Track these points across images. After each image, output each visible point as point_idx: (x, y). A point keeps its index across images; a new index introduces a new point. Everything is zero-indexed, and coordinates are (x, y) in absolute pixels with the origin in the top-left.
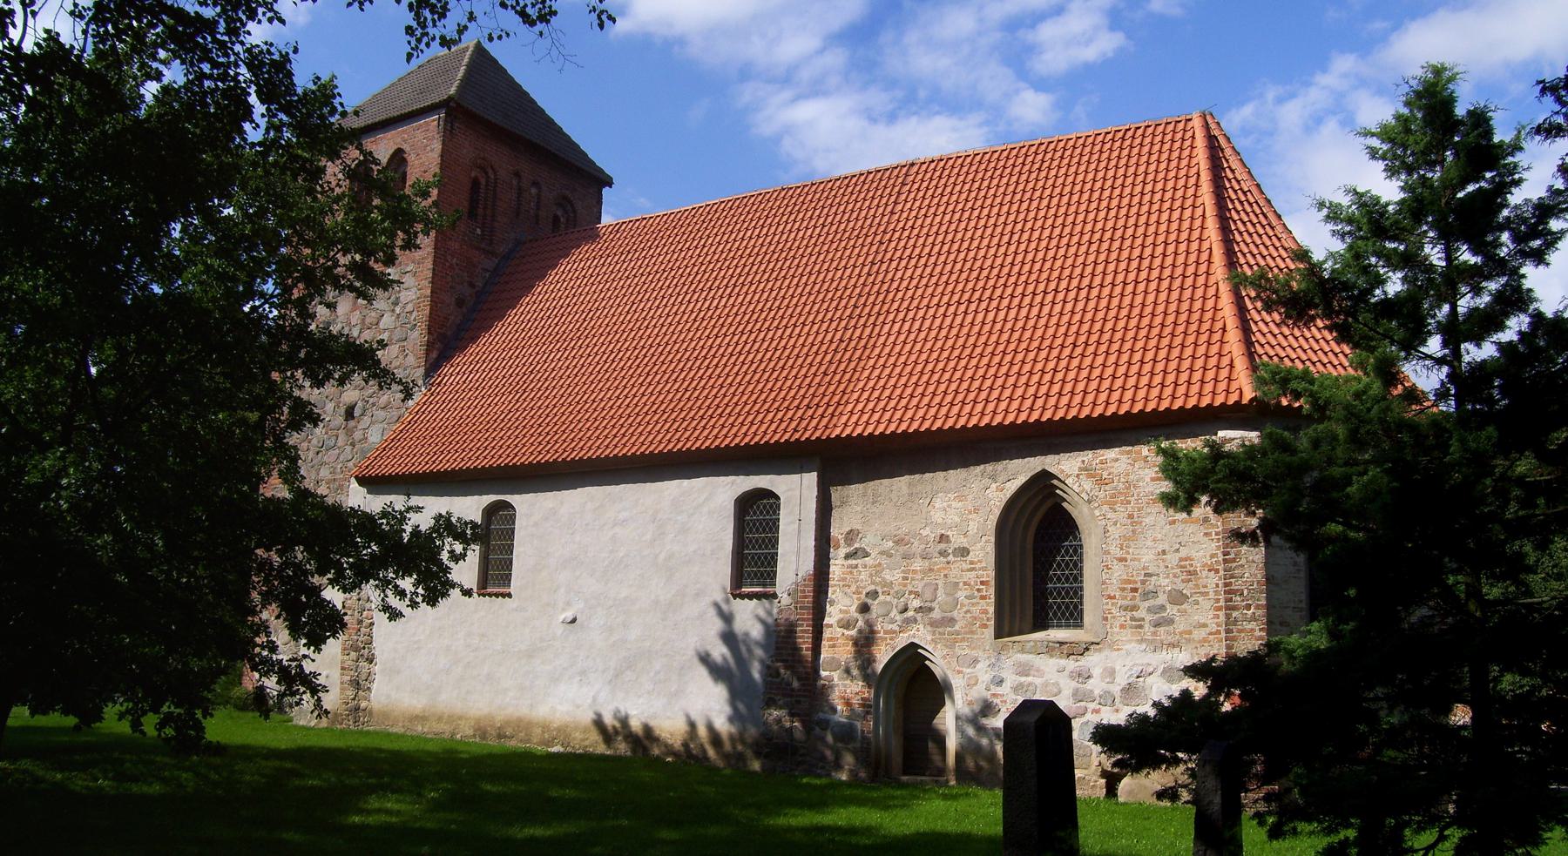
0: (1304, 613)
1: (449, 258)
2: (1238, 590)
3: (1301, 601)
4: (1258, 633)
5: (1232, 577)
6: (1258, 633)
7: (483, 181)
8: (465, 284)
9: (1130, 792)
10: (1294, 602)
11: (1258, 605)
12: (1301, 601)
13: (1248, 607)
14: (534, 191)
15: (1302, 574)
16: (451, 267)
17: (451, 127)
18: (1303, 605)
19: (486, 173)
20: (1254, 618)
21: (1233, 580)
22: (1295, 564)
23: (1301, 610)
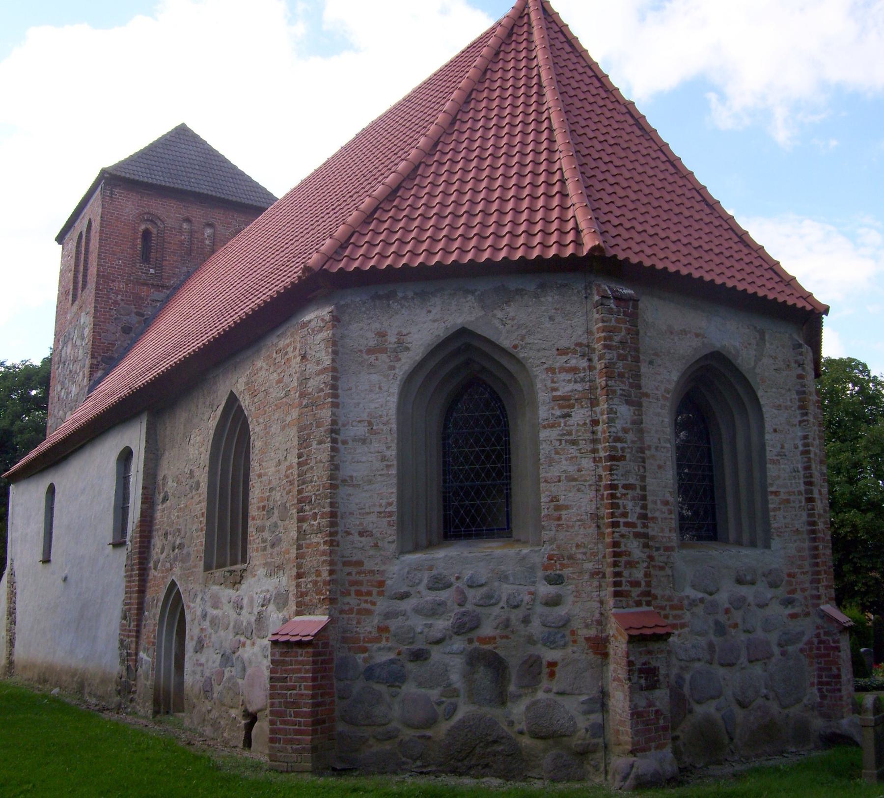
0: (394, 518)
1: (112, 296)
2: (307, 497)
3: (390, 504)
4: (323, 548)
5: (304, 483)
6: (323, 548)
7: (154, 231)
8: (133, 315)
9: (674, 642)
10: (381, 505)
11: (323, 513)
12: (390, 504)
13: (315, 517)
14: (208, 231)
15: (394, 471)
16: (116, 303)
17: (111, 193)
18: (393, 508)
19: (156, 224)
20: (319, 531)
21: (304, 486)
22: (384, 459)
23: (390, 514)
